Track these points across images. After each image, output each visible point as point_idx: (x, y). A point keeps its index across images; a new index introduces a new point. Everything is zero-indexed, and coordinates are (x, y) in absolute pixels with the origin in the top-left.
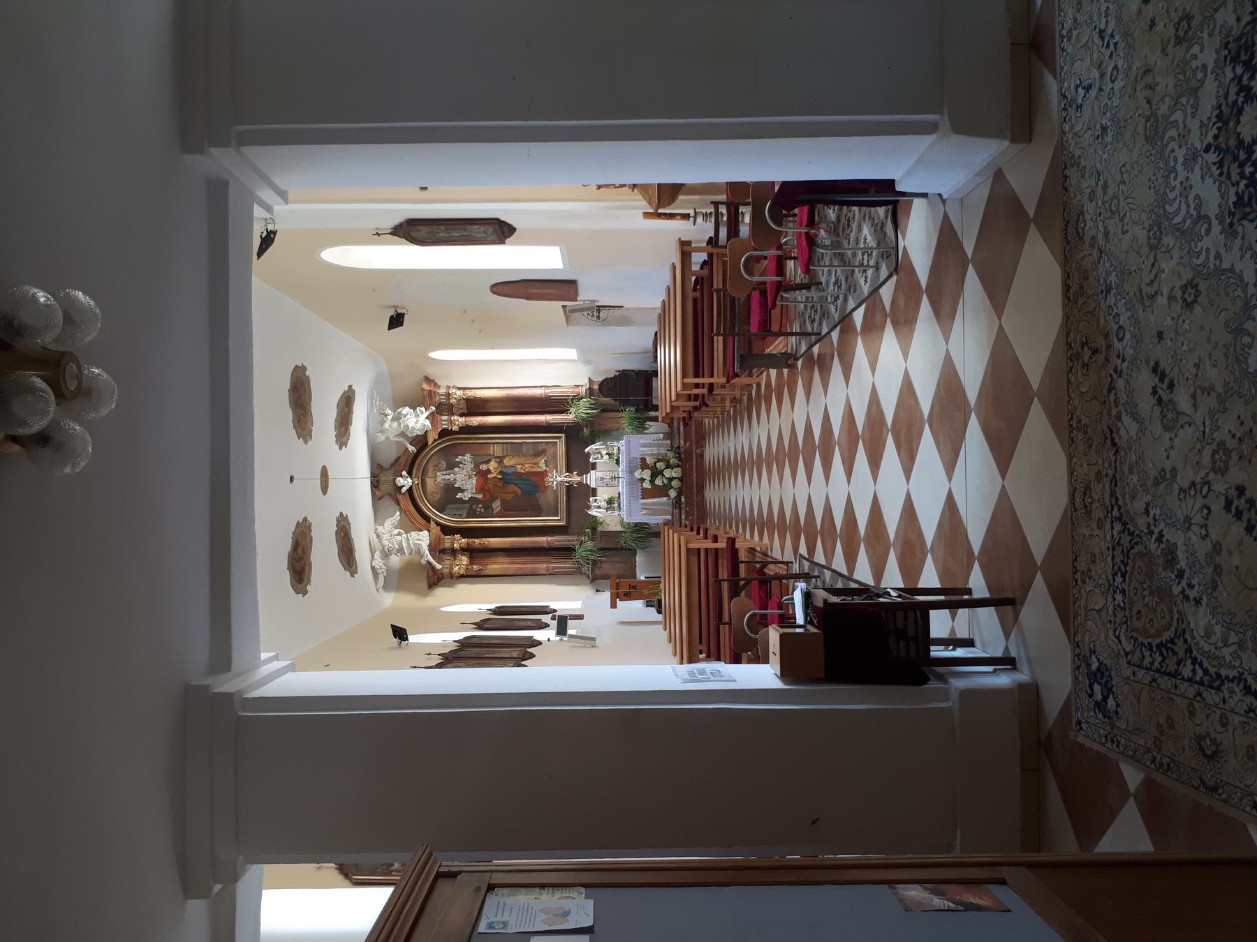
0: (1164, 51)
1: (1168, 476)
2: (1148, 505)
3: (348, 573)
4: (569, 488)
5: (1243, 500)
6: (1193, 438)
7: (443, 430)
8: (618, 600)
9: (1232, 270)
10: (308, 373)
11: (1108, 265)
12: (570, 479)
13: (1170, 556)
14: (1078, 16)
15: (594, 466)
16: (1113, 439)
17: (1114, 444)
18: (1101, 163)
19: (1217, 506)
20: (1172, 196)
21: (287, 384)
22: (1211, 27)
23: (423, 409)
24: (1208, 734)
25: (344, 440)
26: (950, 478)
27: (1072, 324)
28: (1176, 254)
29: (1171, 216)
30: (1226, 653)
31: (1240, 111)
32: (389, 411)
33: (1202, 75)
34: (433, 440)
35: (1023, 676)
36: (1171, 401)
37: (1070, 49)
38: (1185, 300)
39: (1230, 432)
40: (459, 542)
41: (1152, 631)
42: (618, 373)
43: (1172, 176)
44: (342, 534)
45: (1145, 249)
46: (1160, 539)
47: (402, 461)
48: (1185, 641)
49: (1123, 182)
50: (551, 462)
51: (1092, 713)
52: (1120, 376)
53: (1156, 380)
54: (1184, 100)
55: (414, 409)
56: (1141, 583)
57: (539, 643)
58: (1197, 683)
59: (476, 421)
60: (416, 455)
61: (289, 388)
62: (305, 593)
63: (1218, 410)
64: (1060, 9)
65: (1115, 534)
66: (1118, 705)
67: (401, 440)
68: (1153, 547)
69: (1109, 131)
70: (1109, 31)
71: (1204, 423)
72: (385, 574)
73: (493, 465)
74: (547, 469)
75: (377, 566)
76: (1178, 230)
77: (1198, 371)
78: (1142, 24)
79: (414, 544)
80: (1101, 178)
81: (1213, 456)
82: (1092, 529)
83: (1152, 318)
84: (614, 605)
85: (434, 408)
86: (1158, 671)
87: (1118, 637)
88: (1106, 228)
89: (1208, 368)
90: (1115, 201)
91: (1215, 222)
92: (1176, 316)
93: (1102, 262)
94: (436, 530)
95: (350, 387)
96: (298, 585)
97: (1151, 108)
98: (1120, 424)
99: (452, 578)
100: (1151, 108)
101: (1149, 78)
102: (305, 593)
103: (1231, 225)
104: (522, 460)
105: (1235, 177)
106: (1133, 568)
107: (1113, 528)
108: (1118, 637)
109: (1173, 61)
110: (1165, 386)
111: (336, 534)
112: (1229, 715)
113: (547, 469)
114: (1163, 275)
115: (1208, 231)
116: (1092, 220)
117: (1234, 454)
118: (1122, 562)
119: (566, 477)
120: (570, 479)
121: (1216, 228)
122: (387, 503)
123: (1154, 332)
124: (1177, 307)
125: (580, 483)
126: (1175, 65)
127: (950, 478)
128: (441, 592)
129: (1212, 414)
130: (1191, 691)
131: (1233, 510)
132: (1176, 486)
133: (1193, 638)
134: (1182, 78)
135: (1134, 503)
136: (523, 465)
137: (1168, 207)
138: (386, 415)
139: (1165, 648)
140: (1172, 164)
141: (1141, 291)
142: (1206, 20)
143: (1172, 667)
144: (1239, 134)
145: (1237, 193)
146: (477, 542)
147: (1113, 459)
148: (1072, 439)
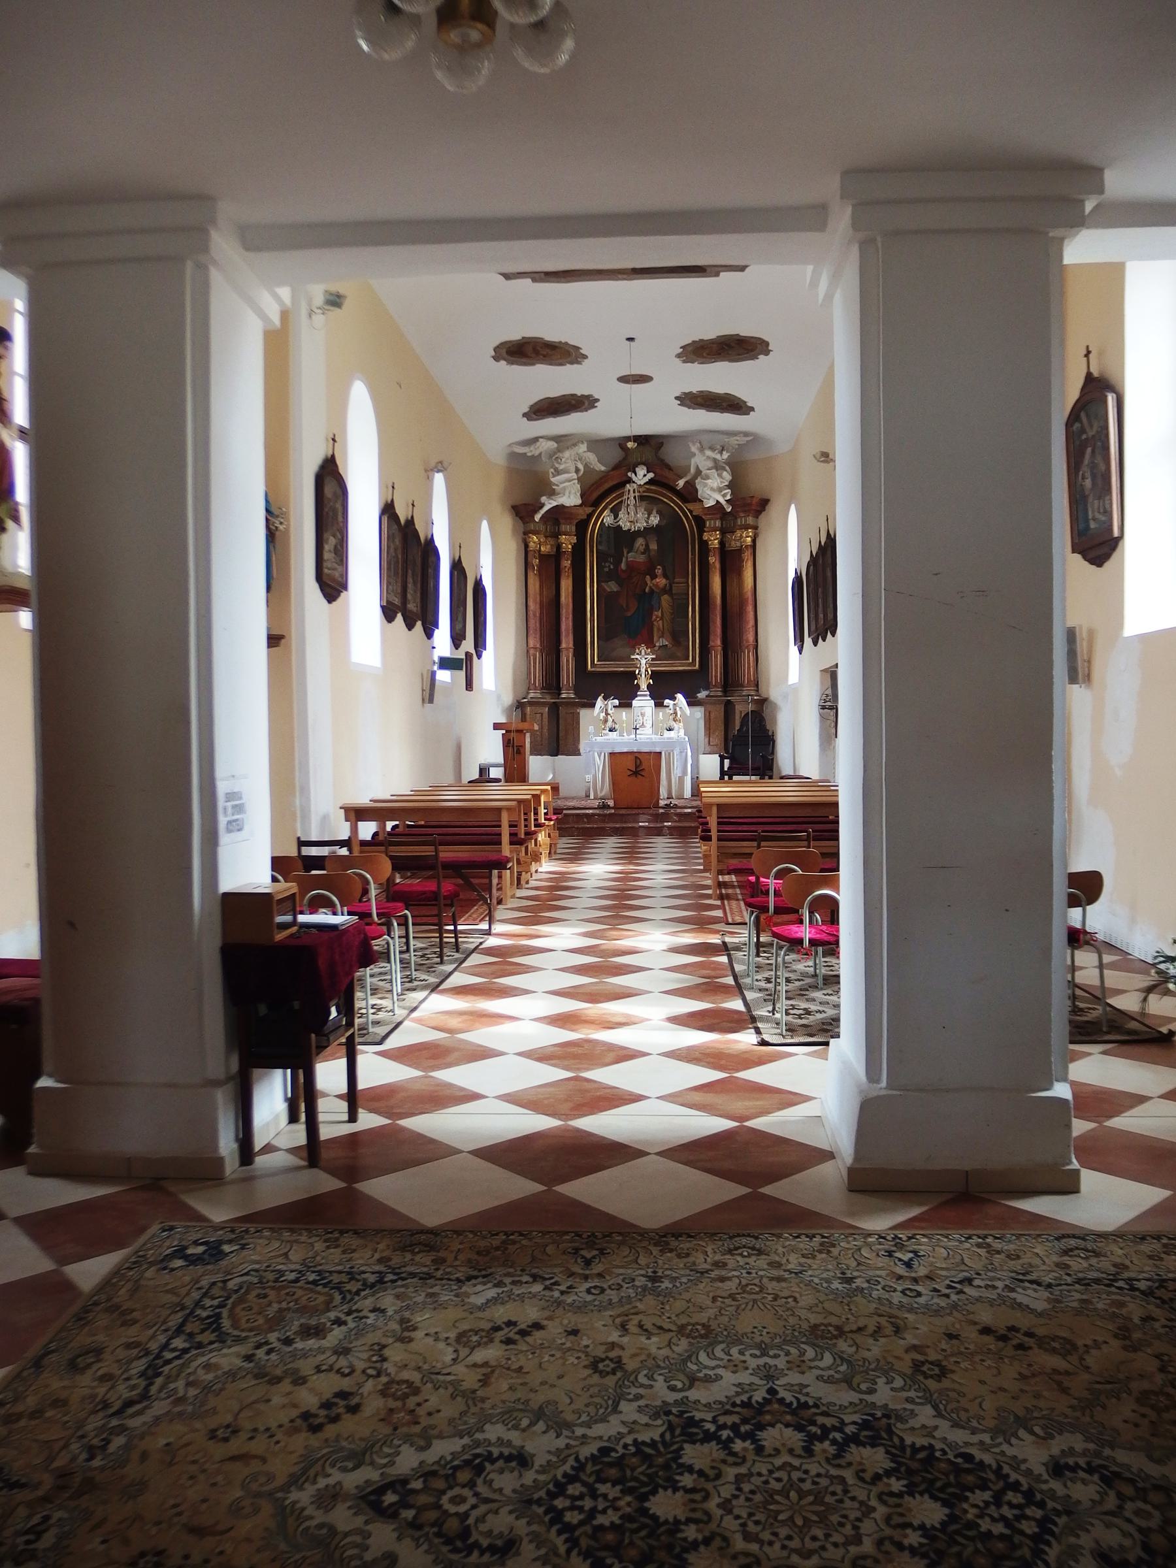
0: (915, 1348)
1: (406, 1334)
2: (383, 1311)
3: (526, 410)
4: (633, 676)
5: (341, 1410)
6: (437, 1362)
7: (704, 522)
8: (504, 732)
9: (615, 1410)
10: (761, 357)
11: (684, 1280)
12: (643, 676)
13: (318, 1332)
14: (1002, 1256)
15: (659, 704)
16: (476, 1277)
17: (469, 1279)
18: (811, 1276)
19: (346, 1384)
20: (734, 1351)
21: (745, 331)
22: (918, 1400)
23: (728, 497)
24: (99, 1361)
25: (688, 402)
26: (499, 1097)
27: (633, 1238)
28: (665, 1352)
29: (709, 1350)
30: (180, 1384)
31: (799, 1428)
32: (725, 455)
33: (864, 1389)
34: (692, 508)
35: (231, 1164)
36: (491, 1341)
37: (967, 1245)
38: (603, 1360)
39: (426, 1401)
40: (568, 542)
41: (238, 1309)
42: (770, 734)
43: (758, 1353)
44: (573, 402)
45: (683, 1320)
46: (339, 1322)
47: (666, 473)
48: (211, 1343)
49: (775, 1299)
50: (663, 654)
51: (175, 1243)
52: (546, 1288)
53: (523, 1326)
54: (843, 1368)
55: (728, 487)
56: (296, 1301)
57: (429, 634)
58: (161, 1351)
59: (714, 560)
60: (673, 489)
61: (742, 334)
62: (497, 358)
63: (456, 1390)
64: (1019, 1236)
65: (364, 1276)
66: (173, 1270)
67: (693, 470)
68: (332, 1315)
69: (845, 1285)
70: (967, 1290)
71: (448, 1374)
72: (529, 454)
73: (661, 581)
74: (656, 648)
75: (538, 444)
76: (690, 1357)
77: (512, 1370)
78: (957, 1326)
79: (564, 488)
80: (793, 1275)
81: (407, 1381)
82: (382, 1251)
83: (599, 1324)
84: (497, 726)
85: (729, 510)
86: (192, 1312)
87: (247, 1274)
88: (729, 1279)
89: (510, 1381)
90: (757, 1289)
91: (678, 1396)
92: (588, 1350)
93: (691, 1273)
94: (582, 513)
95: (752, 409)
96: (504, 350)
97: (851, 1331)
98: (490, 1285)
99: (525, 533)
100: (850, 1332)
101: (889, 1330)
102: (497, 358)
103: (668, 1413)
104: (667, 617)
105: (722, 1420)
106: (319, 1293)
107: (373, 1273)
108: (247, 1274)
109: (897, 1357)
110: (511, 1335)
111: (572, 395)
112: (109, 1384)
113: (656, 648)
114: (643, 1339)
115: (672, 1389)
116: (747, 1264)
117: (399, 1404)
118: (330, 1282)
119: (646, 671)
120: (643, 676)
121: (672, 1397)
122: (616, 455)
123: (580, 1326)
124: (600, 1352)
125: (638, 687)
126: (890, 1359)
127: (499, 1097)
128: (507, 522)
129: (455, 1384)
130: (154, 1346)
131: (335, 1400)
132: (390, 1340)
133: (211, 1351)
134: (871, 1367)
135: (392, 1297)
136: (662, 619)
137: (723, 1346)
138: (721, 453)
139: (214, 1322)
140: (771, 1353)
141: (636, 1314)
142: (928, 1395)
143: (188, 1328)
144: (773, 1426)
145: (703, 1420)
146: (566, 563)
147: (452, 1277)
148: (497, 1234)
